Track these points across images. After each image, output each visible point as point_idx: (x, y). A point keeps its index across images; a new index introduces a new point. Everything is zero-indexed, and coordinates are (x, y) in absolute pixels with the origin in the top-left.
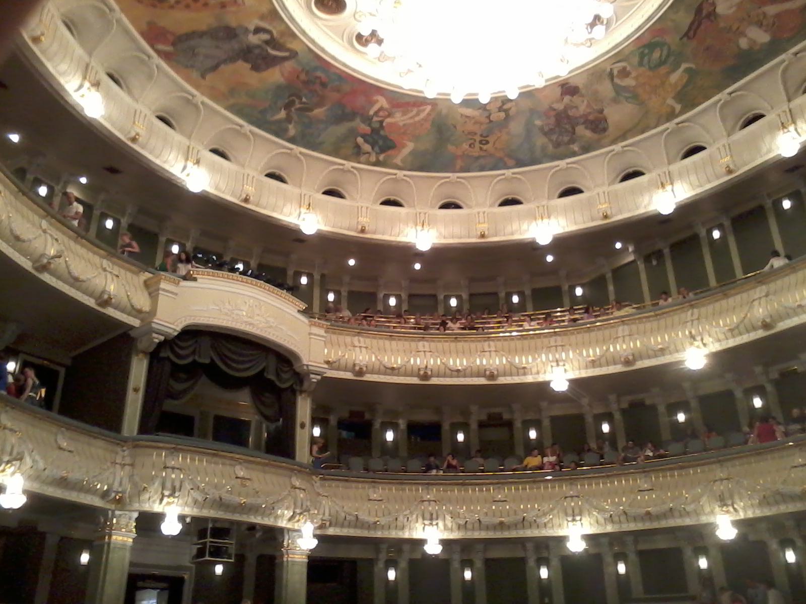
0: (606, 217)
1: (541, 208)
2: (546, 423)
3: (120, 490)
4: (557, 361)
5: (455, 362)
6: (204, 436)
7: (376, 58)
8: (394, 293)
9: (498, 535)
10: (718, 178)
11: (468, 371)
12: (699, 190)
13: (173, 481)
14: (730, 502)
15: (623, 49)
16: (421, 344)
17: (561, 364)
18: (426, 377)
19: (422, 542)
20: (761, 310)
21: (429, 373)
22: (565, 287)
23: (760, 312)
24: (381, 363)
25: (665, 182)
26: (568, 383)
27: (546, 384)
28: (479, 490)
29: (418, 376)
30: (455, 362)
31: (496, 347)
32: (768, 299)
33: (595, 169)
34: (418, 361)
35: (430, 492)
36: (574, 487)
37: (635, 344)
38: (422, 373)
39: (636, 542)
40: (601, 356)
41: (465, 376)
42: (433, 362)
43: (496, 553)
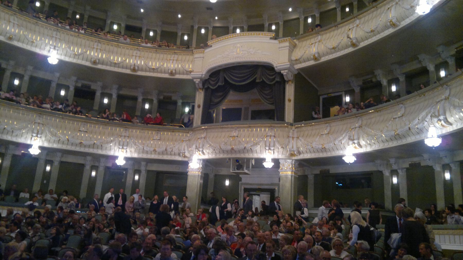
2: (26, 78)
3: (292, 150)
4: (55, 47)
5: (152, 64)
6: (246, 119)
8: (153, 29)
9: (78, 149)
11: (159, 70)
13: (270, 142)
14: (201, 150)
16: (135, 52)
17: (57, 48)
18: (134, 70)
19: (116, 158)
20: (314, 50)
21: (136, 68)
22: (180, 34)
24: (146, 66)
26: (58, 60)
27: (46, 57)
28: (54, 120)
29: (168, 73)
30: (152, 64)
31: (101, 47)
32: (320, 43)
34: (131, 61)
35: (127, 132)
36: (41, 118)
37: (102, 56)
38: (132, 67)
39: (147, 165)
41: (119, 67)
42: (140, 62)
43: (71, 159)
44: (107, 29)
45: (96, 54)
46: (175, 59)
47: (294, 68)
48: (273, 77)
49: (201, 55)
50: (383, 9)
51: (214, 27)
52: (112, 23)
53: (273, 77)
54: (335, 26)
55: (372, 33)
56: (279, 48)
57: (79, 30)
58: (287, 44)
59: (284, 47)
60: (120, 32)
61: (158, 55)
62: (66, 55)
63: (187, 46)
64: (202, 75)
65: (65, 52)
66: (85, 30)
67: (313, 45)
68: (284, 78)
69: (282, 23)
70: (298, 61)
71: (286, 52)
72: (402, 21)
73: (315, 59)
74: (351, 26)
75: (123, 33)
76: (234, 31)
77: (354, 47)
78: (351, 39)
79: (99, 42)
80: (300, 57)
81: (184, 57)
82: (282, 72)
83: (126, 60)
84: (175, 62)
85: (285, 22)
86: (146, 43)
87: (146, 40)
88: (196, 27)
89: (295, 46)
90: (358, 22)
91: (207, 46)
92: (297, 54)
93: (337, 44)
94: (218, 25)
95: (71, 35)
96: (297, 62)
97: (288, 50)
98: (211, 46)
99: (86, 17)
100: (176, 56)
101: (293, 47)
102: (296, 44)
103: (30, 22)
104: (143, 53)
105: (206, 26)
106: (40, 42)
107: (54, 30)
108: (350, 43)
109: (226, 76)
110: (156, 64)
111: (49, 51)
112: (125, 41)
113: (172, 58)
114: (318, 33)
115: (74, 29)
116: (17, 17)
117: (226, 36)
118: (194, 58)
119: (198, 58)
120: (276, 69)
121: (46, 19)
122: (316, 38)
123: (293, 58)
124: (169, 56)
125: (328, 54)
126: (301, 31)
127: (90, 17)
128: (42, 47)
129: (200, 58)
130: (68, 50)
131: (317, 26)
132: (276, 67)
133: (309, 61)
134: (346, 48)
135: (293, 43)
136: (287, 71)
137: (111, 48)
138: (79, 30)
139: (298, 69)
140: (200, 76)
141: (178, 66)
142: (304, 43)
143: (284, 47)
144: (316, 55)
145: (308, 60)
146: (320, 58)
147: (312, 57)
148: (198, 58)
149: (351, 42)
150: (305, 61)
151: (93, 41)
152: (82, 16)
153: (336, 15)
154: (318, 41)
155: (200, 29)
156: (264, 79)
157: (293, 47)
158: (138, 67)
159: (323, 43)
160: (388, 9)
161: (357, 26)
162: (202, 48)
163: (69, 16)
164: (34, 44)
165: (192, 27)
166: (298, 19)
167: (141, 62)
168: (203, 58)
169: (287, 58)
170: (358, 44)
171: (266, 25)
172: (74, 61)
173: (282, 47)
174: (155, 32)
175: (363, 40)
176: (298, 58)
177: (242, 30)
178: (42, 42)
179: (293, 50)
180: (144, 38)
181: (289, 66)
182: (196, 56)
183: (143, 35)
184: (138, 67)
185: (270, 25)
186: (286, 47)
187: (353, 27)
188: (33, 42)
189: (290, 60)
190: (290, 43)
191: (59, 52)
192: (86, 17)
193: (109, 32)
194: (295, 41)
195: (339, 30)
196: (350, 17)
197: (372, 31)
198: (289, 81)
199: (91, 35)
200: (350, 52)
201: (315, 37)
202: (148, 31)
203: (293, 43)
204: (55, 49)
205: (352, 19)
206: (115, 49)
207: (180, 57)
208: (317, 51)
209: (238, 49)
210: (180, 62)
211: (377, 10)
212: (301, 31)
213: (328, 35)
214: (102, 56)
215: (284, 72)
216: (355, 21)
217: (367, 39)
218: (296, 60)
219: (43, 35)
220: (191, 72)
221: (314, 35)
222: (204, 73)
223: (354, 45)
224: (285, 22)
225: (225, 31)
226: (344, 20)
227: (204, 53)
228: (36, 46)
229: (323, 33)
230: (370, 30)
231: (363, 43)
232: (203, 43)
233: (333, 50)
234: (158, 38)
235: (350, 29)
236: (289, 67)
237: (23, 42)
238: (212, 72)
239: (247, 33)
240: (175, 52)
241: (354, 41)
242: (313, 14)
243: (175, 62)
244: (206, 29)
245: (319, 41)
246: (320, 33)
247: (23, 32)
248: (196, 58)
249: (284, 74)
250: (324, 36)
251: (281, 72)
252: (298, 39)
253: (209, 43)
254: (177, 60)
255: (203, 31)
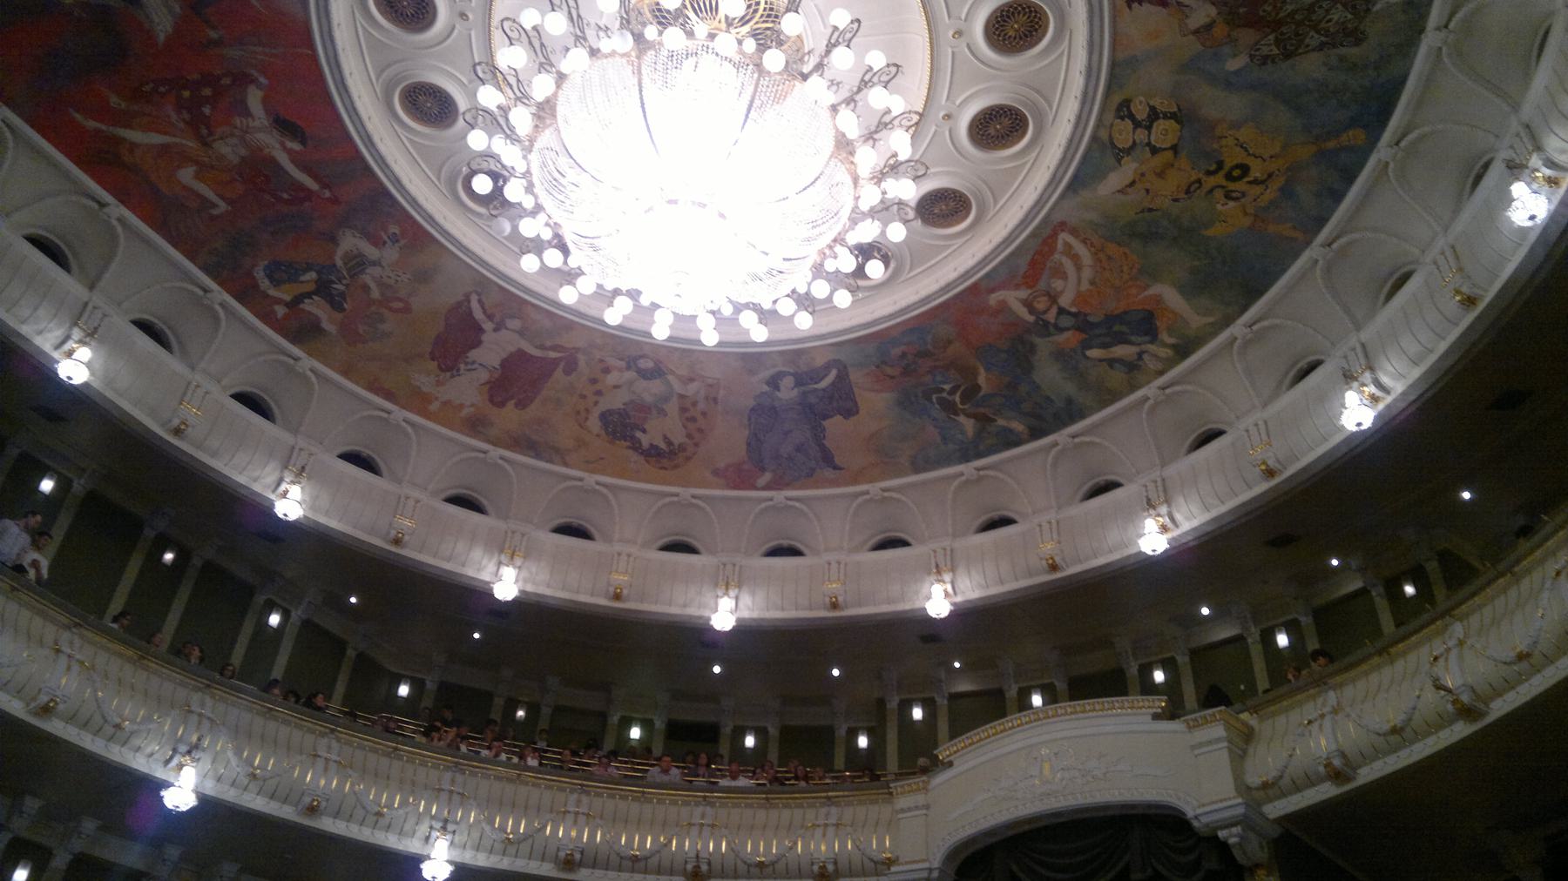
0: (835, 606)
1: (729, 567)
4: (446, 821)
5: (755, 847)
7: (731, 301)
10: (1030, 574)
12: (995, 590)
15: (437, 241)
17: (450, 827)
20: (1323, 743)
21: (704, 868)
22: (841, 732)
23: (315, 779)
25: (942, 565)
30: (755, 847)
33: (830, 514)
37: (592, 836)
38: (689, 867)
40: (653, 853)
44: (609, 744)
45: (573, 834)
46: (833, 820)
47: (1262, 815)
48: (1192, 857)
49: (920, 799)
50: (1536, 575)
51: (954, 697)
52: (627, 723)
53: (1192, 857)
54: (1380, 653)
55: (1524, 665)
56: (1193, 747)
57: (522, 757)
58: (1218, 731)
59: (1210, 742)
60: (649, 750)
61: (774, 814)
62: (477, 849)
63: (868, 770)
64: (931, 870)
65: (476, 835)
66: (540, 754)
67: (1316, 725)
68: (1233, 858)
69: (1187, 659)
70: (1271, 789)
71: (1221, 757)
72: (1492, 699)
73: (1337, 776)
74: (1438, 647)
75: (658, 749)
76: (1025, 705)
77: (1475, 720)
78: (1449, 691)
79: (584, 790)
80: (1274, 773)
81: (861, 811)
82: (1222, 834)
83: (670, 842)
84: (831, 830)
85: (1196, 654)
86: (734, 778)
87: (734, 767)
88: (893, 704)
89: (1248, 736)
90: (1458, 629)
91: (935, 765)
92: (1265, 763)
93: (1403, 717)
94: (964, 686)
95: (498, 778)
96: (1270, 792)
97: (1225, 754)
98: (951, 764)
99: (546, 711)
100: (834, 810)
101: (1244, 740)
102: (1251, 729)
103: (376, 751)
104: (598, 802)
105: (926, 695)
106: (401, 812)
107: (447, 768)
108: (1450, 707)
109: (1015, 868)
110: (768, 847)
111: (427, 839)
112: (666, 778)
113: (821, 821)
114: (1320, 682)
115: (503, 757)
116: (338, 740)
117: (998, 725)
118: (898, 812)
119: (910, 810)
120: (1196, 824)
121: (426, 734)
122: (1320, 701)
123: (1254, 780)
124: (810, 814)
125: (1377, 754)
126: (1262, 682)
127: (559, 710)
128: (407, 827)
129: (917, 808)
130: (487, 828)
131: (1315, 655)
132: (1196, 817)
133: (1314, 785)
134: (1430, 734)
135: (1238, 725)
136: (1236, 830)
137: (622, 805)
138: (522, 757)
139: (1280, 820)
140: (925, 874)
141: (843, 845)
142: (1281, 720)
143: (1210, 742)
144: (1337, 762)
145: (1310, 781)
146: (1355, 769)
147: (1321, 769)
148: (910, 810)
149: (1454, 702)
150: (1297, 788)
151: (563, 790)
152: (533, 710)
153: (1373, 613)
154: (1327, 709)
155: (906, 706)
156: (1160, 868)
157: (1244, 740)
158: (709, 864)
159: (1348, 716)
160: (1558, 573)
161: (1461, 643)
162: (924, 771)
163: (496, 715)
164: (383, 822)
165: (881, 703)
166: (1239, 639)
167: (718, 846)
168: (927, 807)
169: (1231, 780)
170: (1482, 706)
171: (1133, 670)
172: (504, 864)
173: (1201, 745)
174: (761, 734)
175: (1498, 693)
176: (1271, 775)
177: (1051, 697)
178: (410, 809)
179: (1245, 752)
180: (726, 760)
181: (1241, 810)
182: (903, 802)
183: (724, 748)
184: (709, 864)
185: (1146, 671)
186: (1218, 740)
187: (1448, 650)
188: (379, 814)
189: (1243, 788)
190: (1228, 727)
191: (457, 838)
192: (546, 711)
193: (613, 754)
194: (1245, 716)
195: (1400, 665)
196: (1425, 617)
197: (1522, 657)
198: (1258, 866)
199: (560, 769)
200: (1527, 704)
201: (1314, 697)
202: (740, 734)
203: (1238, 725)
204: (444, 828)
205: (1433, 621)
206: (635, 808)
207: (848, 813)
208: (1334, 747)
209: (1046, 766)
210: (849, 829)
211: (1518, 581)
212: (1262, 682)
213: (1361, 685)
214: (592, 836)
215: (1231, 836)
216: (1446, 627)
217: (1510, 685)
218: (1265, 786)
219: (411, 787)
220: (889, 863)
221: (1312, 691)
222: (936, 864)
223: (1467, 713)
224: (1196, 654)
225: (991, 707)
226: (1403, 630)
227: (926, 790)
228: (388, 828)
229: (1338, 679)
230: (1513, 654)
231: (1539, 676)
232: (920, 757)
233: (1394, 739)
234: (773, 755)
235: (1436, 659)
236: (1244, 815)
237: (350, 819)
238: (963, 856)
239: (1068, 706)
240: (829, 798)
241: (1465, 698)
242: (1290, 617)
243: (831, 830)
244: (928, 705)
245: (1335, 711)
246: (1331, 681)
247: (352, 785)
248: (902, 811)
249: (1232, 841)
250: (1349, 691)
251: (1216, 837)
252: (1254, 710)
253: (942, 753)
254: (837, 825)
255: (917, 713)
